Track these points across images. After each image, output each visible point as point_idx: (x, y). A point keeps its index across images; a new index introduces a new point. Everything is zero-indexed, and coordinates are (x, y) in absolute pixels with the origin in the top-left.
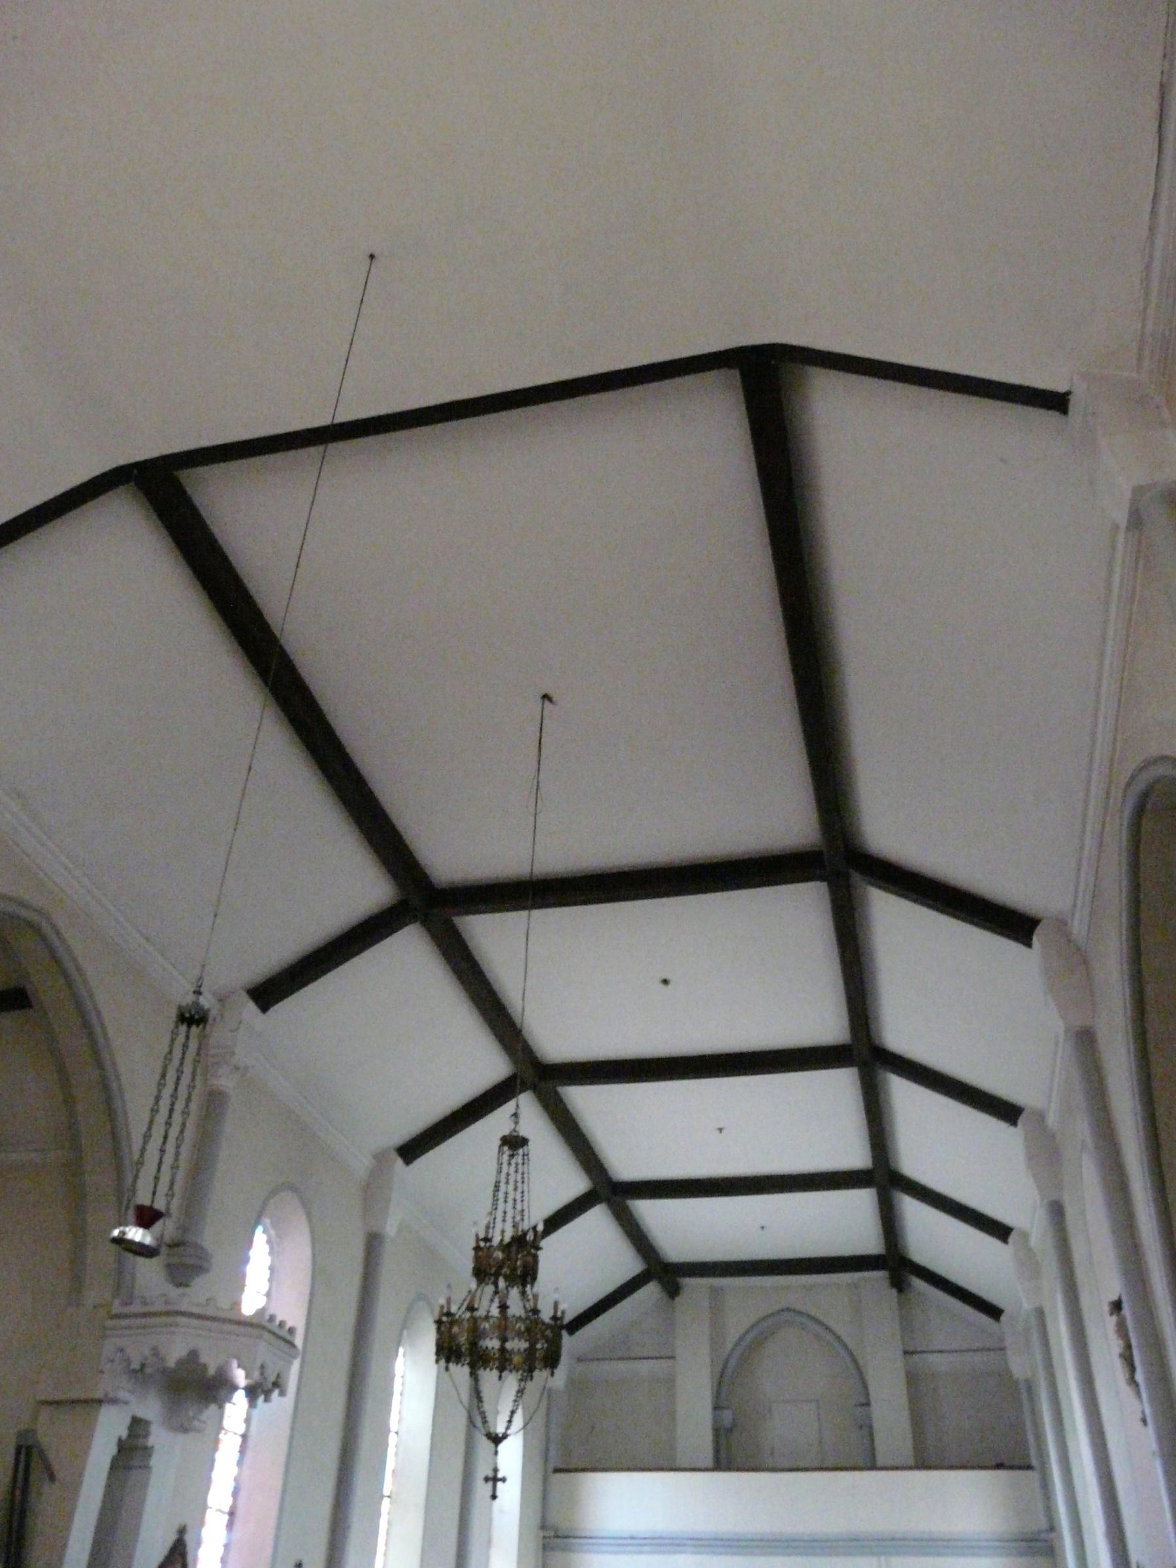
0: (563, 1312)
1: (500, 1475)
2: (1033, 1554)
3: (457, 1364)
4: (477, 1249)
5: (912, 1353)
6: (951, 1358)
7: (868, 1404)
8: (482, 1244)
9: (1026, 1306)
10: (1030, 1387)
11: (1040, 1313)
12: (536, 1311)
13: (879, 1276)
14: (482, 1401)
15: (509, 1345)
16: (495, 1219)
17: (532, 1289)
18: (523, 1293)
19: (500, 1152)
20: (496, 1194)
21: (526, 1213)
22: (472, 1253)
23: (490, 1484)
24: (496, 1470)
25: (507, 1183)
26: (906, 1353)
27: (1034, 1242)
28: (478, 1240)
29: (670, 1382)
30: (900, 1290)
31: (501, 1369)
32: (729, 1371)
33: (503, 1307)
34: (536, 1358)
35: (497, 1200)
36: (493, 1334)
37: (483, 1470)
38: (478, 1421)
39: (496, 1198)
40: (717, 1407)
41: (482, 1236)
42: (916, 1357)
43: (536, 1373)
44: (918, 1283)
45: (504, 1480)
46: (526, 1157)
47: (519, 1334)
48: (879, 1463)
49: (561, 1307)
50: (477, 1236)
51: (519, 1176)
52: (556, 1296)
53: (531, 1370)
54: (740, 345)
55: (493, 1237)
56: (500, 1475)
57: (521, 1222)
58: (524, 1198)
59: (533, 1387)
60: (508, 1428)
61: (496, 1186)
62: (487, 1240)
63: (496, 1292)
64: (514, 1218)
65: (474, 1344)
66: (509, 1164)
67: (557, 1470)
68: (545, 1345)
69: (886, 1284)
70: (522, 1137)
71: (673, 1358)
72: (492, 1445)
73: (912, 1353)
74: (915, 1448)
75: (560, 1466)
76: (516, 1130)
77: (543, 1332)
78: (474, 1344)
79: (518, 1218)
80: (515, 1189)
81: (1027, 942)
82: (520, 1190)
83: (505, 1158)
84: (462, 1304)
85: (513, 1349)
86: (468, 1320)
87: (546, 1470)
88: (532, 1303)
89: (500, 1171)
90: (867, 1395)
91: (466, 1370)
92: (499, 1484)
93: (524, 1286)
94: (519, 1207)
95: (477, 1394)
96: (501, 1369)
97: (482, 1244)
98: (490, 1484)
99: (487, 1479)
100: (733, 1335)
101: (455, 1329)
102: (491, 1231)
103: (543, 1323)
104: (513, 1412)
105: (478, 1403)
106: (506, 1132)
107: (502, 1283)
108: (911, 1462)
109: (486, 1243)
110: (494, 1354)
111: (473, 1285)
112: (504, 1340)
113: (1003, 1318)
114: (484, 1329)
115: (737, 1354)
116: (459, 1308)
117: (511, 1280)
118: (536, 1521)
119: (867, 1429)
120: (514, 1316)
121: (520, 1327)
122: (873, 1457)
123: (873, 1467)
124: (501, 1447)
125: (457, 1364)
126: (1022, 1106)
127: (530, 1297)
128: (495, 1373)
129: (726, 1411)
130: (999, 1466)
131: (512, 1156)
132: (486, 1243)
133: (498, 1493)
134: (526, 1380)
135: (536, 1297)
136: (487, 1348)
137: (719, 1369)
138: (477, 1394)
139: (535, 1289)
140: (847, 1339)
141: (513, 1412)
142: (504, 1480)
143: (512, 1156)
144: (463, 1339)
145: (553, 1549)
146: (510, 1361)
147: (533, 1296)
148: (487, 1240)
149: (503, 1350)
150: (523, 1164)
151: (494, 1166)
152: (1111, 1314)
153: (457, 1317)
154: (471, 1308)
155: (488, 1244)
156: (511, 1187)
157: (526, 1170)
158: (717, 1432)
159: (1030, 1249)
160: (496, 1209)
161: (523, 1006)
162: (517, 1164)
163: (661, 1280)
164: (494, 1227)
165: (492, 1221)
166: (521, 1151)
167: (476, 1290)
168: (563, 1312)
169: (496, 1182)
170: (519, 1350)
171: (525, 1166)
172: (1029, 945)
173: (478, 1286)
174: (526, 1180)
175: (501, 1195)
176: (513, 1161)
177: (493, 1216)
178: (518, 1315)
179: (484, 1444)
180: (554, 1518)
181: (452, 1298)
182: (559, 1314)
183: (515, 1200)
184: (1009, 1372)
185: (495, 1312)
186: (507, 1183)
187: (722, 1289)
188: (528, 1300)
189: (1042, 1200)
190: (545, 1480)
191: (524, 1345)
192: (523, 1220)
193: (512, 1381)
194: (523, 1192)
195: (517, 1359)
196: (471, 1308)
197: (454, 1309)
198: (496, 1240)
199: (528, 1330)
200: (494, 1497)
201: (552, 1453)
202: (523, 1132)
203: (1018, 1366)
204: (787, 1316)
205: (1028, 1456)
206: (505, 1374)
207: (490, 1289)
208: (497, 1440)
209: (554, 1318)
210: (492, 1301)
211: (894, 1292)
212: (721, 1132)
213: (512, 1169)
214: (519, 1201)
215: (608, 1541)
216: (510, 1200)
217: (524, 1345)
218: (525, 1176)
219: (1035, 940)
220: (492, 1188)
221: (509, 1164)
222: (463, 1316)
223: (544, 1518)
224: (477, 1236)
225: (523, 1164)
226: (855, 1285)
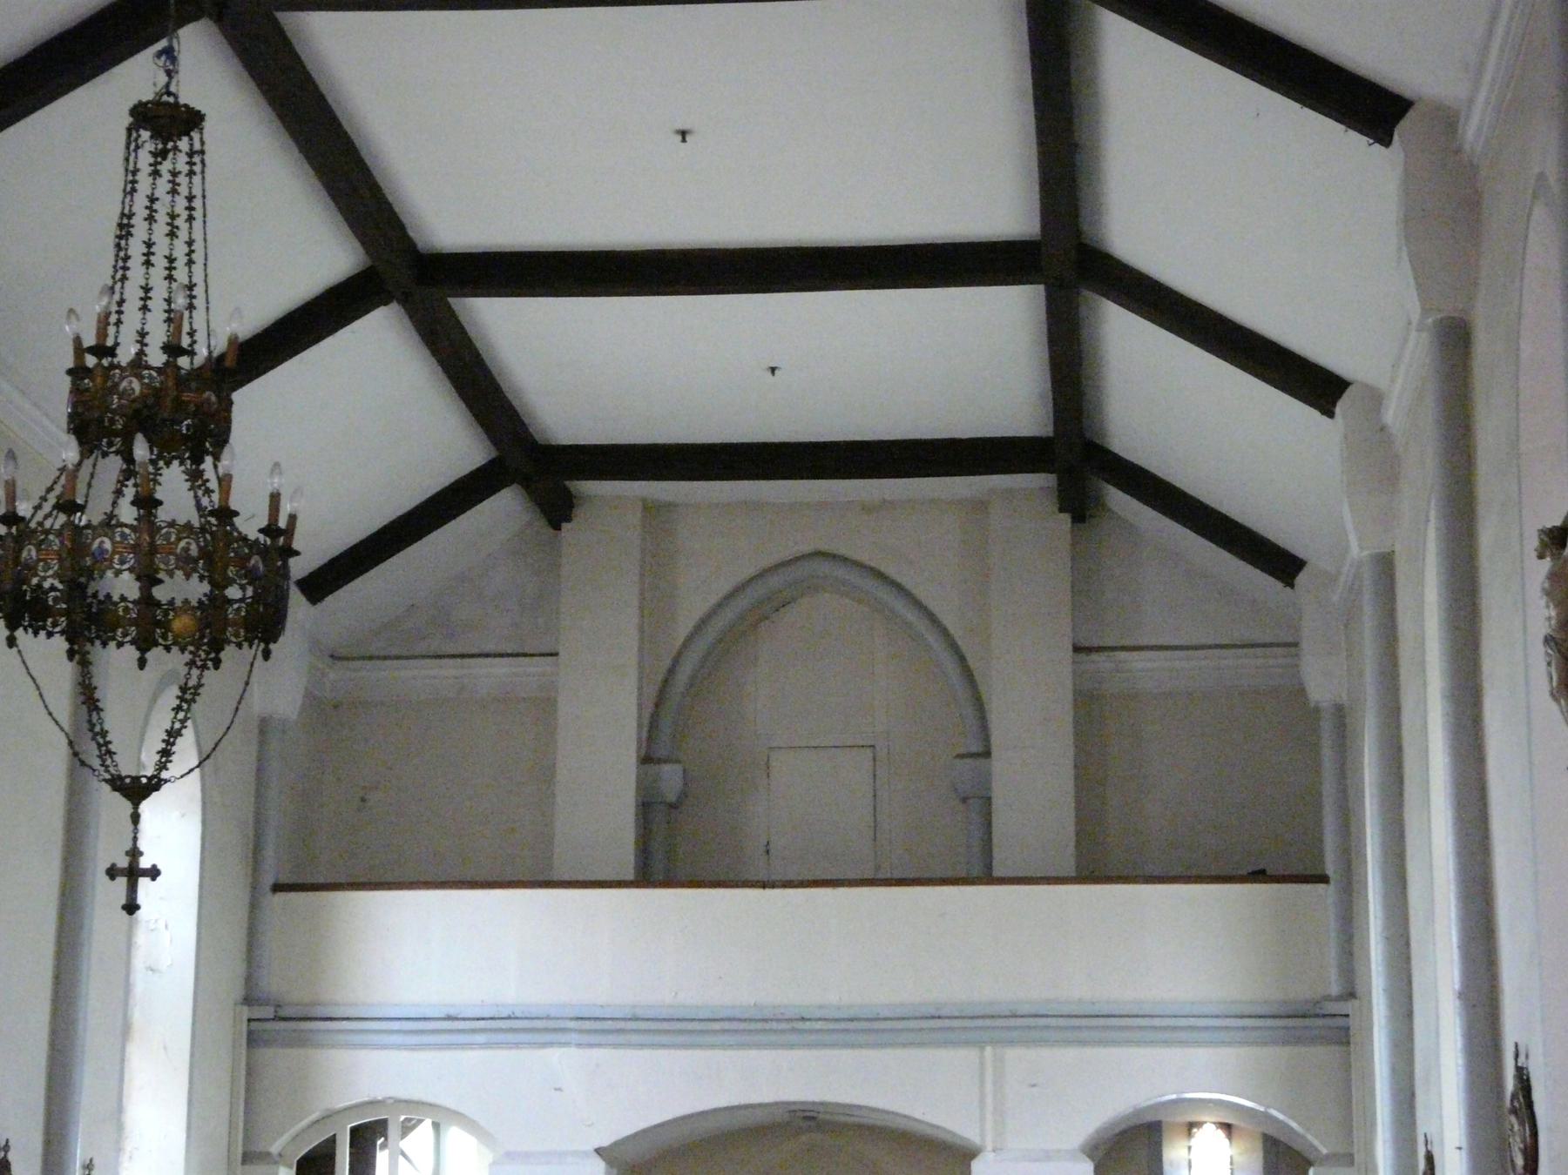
0: (293, 518)
1: (145, 863)
2: (1298, 1041)
3: (36, 633)
4: (78, 372)
5: (1090, 650)
6: (1178, 661)
7: (987, 754)
8: (91, 361)
9: (1357, 551)
10: (1342, 717)
11: (1385, 565)
12: (226, 514)
13: (1036, 484)
14: (99, 710)
15: (160, 593)
16: (121, 302)
17: (216, 467)
18: (195, 476)
19: (132, 146)
20: (123, 243)
21: (199, 291)
22: (67, 382)
23: (122, 882)
24: (135, 853)
25: (151, 219)
26: (1077, 649)
27: (1391, 415)
28: (79, 350)
29: (544, 706)
30: (1079, 517)
31: (144, 644)
32: (682, 677)
33: (147, 503)
34: (226, 623)
35: (127, 258)
36: (122, 562)
37: (107, 850)
38: (91, 753)
39: (122, 254)
40: (646, 759)
41: (89, 340)
42: (1101, 661)
43: (229, 654)
44: (1119, 500)
45: (154, 873)
46: (197, 159)
47: (187, 564)
48: (997, 873)
49: (286, 508)
50: (77, 341)
51: (181, 203)
52: (276, 482)
53: (217, 646)
54: (656, 442)
55: (117, 344)
56: (145, 863)
57: (186, 314)
58: (194, 256)
59: (219, 684)
60: (162, 766)
61: (121, 226)
62: (101, 350)
63: (128, 473)
64: (169, 301)
65: (76, 588)
66: (156, 174)
67: (278, 888)
68: (250, 592)
69: (1051, 504)
70: (186, 106)
71: (556, 654)
72: (127, 806)
73: (1090, 650)
74: (1079, 821)
75: (285, 879)
76: (173, 89)
77: (242, 561)
78: (76, 588)
79: (180, 301)
80: (172, 235)
81: (1385, 139)
82: (183, 235)
83: (144, 159)
84: (44, 499)
85: (171, 602)
86: (59, 534)
87: (255, 887)
88: (215, 497)
89: (131, 191)
90: (986, 739)
91: (60, 644)
92: (144, 882)
93: (198, 460)
94: (181, 274)
95: (88, 698)
96: (144, 644)
97: (91, 361)
98: (122, 882)
99: (112, 873)
100: (691, 607)
101: (29, 553)
102: (111, 330)
103: (245, 539)
104: (173, 734)
105: (90, 712)
106: (148, 96)
107: (141, 450)
108: (1069, 867)
109: (100, 359)
110: (126, 609)
111: (70, 452)
112: (148, 579)
113: (1302, 579)
114: (102, 551)
115: (701, 646)
116: (37, 508)
117: (166, 448)
118: (230, 985)
119: (980, 803)
120: (172, 524)
121: (186, 550)
122: (989, 866)
123: (988, 877)
124: (146, 807)
125: (36, 633)
126: (1305, 559)
127: (213, 484)
128: (131, 652)
129: (666, 768)
130: (1259, 876)
131: (161, 155)
132: (100, 359)
133: (142, 898)
134: (204, 667)
135: (225, 481)
136: (108, 596)
137: (651, 692)
138: (88, 698)
139: (224, 463)
140: (948, 621)
141: (173, 734)
142: (154, 873)
143: (161, 155)
144: (50, 580)
145: (267, 1043)
146: (166, 626)
147: (220, 480)
148: (101, 350)
149: (147, 601)
150: (191, 173)
151: (118, 180)
152: (1541, 557)
153: (33, 525)
154: (68, 506)
155: (105, 362)
156: (161, 228)
157: (197, 191)
158: (646, 808)
159: (1383, 429)
160: (124, 278)
161: (208, 315)
162: (174, 174)
163: (527, 483)
164: (119, 323)
165: (114, 308)
166: (183, 144)
167: (80, 464)
168: (293, 518)
169: (123, 215)
170: (186, 601)
171: (197, 179)
172: (1329, 413)
173: (85, 454)
174: (198, 214)
175: (136, 248)
176: (165, 167)
177: (117, 297)
178: (182, 521)
179: (113, 804)
180: (273, 983)
181: (19, 483)
182: (282, 523)
183: (171, 260)
184: (1301, 691)
185: (128, 513)
186: (151, 219)
187: (671, 506)
188: (208, 492)
189: (1425, 311)
190: (254, 906)
191: (196, 589)
192: (191, 307)
193: (168, 662)
194: (190, 243)
195: (181, 623)
196: (68, 506)
197: (24, 509)
198: (126, 354)
199: (205, 554)
200: (131, 907)
201: (269, 852)
202: (189, 94)
203: (1323, 683)
204: (824, 568)
205: (1322, 862)
206: (155, 654)
207: (114, 464)
208: (137, 790)
209: (271, 530)
210: (119, 493)
211: (1066, 518)
212: (684, 140)
213: (163, 185)
214: (181, 262)
215: (396, 1025)
216: (159, 261)
217: (196, 589)
218: (197, 203)
219: (1338, 410)
220: (111, 230)
221: (156, 174)
222: (48, 524)
223: (250, 980)
224: (77, 341)
225: (191, 173)
226: (980, 506)
